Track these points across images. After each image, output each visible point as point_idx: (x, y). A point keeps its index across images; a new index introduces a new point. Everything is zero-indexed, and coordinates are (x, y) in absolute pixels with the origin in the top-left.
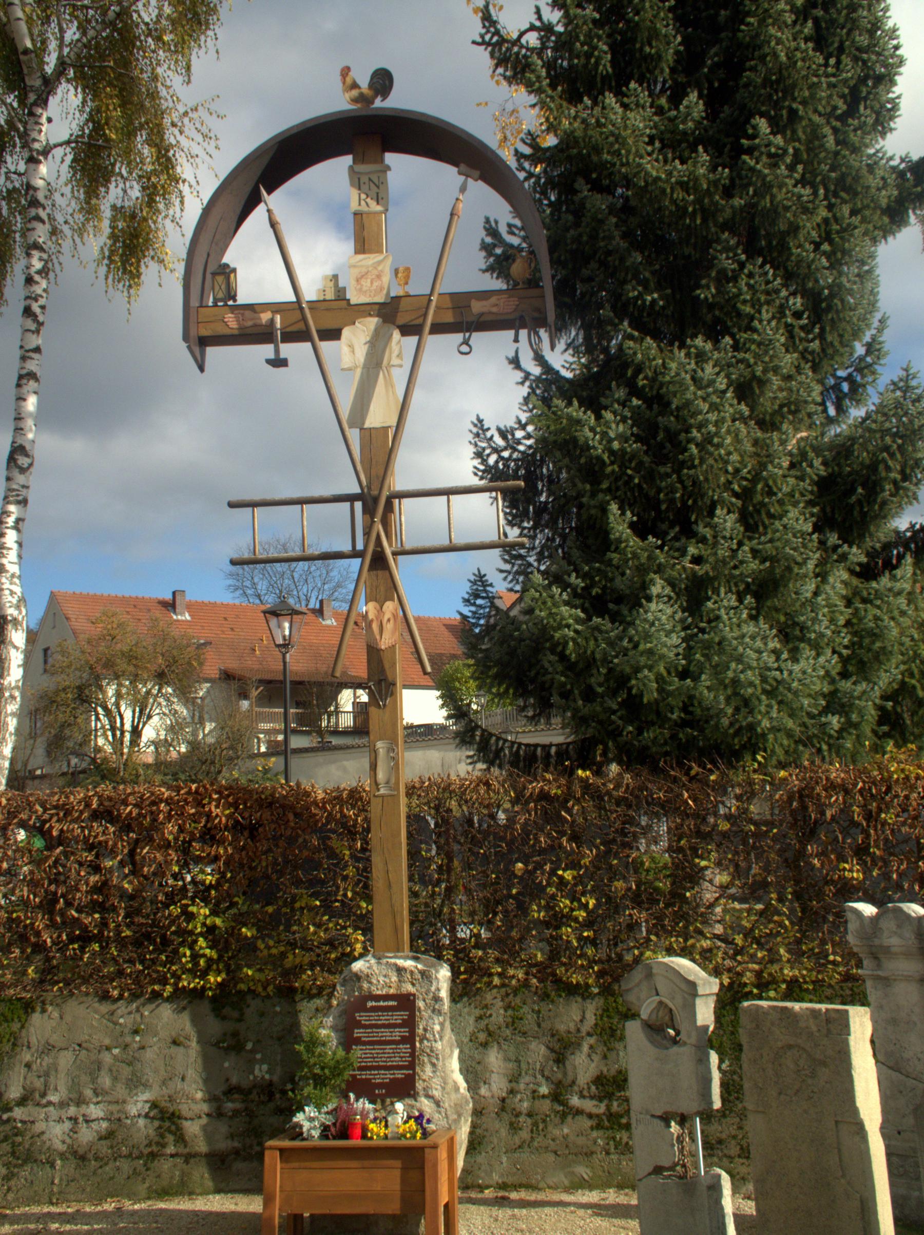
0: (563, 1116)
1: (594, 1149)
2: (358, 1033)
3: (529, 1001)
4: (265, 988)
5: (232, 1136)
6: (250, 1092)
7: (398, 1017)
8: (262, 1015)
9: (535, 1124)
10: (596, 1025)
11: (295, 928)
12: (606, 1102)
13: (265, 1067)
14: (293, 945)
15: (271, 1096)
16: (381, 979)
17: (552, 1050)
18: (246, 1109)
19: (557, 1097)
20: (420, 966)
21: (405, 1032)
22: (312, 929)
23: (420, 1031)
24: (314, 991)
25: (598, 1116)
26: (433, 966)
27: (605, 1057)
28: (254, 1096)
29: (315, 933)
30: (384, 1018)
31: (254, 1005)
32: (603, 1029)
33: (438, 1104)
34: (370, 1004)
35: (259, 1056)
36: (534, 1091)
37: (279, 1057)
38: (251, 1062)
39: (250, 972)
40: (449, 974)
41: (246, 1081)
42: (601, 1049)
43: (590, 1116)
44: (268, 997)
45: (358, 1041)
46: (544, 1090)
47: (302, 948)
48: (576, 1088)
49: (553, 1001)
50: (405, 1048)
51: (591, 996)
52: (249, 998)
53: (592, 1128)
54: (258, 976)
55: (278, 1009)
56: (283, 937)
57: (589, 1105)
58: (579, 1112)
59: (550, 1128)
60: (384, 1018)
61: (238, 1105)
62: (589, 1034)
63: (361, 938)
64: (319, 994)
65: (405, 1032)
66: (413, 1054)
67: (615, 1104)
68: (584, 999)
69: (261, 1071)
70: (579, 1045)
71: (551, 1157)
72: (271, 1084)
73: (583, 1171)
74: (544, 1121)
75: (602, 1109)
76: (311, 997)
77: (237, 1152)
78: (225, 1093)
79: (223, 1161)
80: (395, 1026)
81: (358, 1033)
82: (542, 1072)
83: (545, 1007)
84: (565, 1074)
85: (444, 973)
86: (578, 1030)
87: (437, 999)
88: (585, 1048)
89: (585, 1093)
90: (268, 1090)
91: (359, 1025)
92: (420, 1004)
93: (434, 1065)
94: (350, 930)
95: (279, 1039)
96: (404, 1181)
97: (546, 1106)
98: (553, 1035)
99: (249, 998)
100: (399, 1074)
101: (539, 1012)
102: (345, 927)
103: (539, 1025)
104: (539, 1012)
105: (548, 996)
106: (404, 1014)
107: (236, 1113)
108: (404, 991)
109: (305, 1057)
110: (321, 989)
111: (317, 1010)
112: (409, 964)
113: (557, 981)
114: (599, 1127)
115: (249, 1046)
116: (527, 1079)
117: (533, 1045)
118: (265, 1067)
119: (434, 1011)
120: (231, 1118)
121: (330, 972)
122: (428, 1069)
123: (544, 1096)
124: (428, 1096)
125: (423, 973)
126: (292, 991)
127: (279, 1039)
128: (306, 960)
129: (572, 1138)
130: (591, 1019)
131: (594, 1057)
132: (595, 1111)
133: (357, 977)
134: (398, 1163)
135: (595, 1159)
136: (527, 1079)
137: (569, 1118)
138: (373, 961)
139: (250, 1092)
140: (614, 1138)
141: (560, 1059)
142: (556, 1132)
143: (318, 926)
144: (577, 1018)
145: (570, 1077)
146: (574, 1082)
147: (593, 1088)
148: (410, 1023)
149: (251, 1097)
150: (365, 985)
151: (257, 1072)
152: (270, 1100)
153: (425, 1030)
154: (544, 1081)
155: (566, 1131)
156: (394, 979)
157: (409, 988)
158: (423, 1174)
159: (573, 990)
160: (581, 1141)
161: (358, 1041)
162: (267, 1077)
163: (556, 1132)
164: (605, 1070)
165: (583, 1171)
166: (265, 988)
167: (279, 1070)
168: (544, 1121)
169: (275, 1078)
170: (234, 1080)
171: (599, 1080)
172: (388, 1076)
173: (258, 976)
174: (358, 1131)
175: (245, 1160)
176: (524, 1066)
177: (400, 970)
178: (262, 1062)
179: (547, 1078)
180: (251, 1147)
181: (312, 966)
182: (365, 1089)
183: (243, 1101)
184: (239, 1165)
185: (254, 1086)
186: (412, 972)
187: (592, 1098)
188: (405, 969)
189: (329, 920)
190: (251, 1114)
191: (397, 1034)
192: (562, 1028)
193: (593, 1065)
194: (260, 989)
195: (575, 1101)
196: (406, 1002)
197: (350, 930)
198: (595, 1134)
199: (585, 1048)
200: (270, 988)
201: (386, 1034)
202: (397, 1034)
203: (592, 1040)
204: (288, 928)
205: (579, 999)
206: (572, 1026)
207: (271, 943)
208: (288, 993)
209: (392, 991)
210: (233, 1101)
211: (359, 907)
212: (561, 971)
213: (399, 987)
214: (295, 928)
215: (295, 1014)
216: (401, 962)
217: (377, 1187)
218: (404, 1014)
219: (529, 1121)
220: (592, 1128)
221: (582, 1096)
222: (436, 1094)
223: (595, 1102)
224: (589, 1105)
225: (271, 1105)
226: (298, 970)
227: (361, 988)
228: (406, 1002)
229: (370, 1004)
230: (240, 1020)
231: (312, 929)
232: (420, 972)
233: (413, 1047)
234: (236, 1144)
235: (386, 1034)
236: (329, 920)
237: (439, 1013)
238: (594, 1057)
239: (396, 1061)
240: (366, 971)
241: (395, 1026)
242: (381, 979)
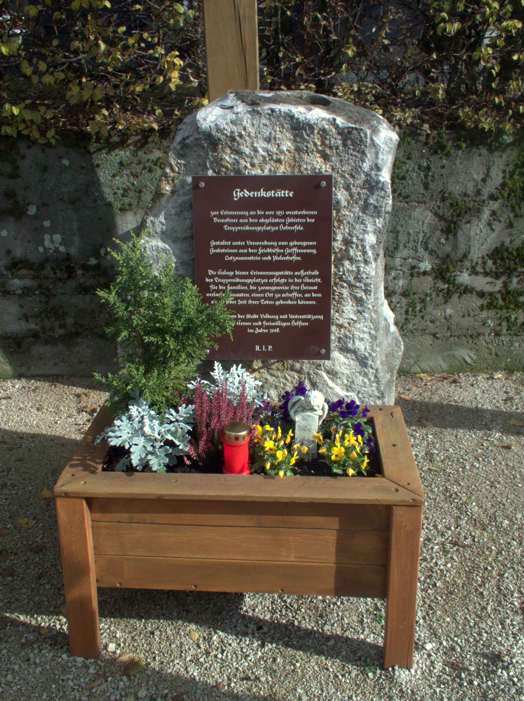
0: (447, 296)
1: (482, 330)
2: (216, 247)
3: (415, 154)
4: (43, 133)
5: (26, 318)
6: (42, 266)
7: (296, 220)
8: (45, 169)
9: (412, 305)
10: (503, 185)
11: (76, 44)
12: (503, 278)
13: (57, 237)
14: (79, 72)
15: (71, 273)
16: (260, 145)
17: (441, 218)
18: (40, 286)
19: (441, 273)
20: (339, 121)
21: (309, 247)
22: (103, 46)
23: (337, 245)
24: (116, 139)
25: (491, 294)
26: (362, 120)
27: (510, 225)
28: (48, 271)
29: (108, 53)
30: (268, 222)
31: (29, 159)
32: (512, 191)
33: (363, 361)
34: (239, 194)
35: (47, 224)
36: (413, 267)
37: (75, 226)
38: (38, 232)
39: (16, 111)
40: (395, 137)
41: (36, 254)
42: (506, 215)
43: (481, 294)
44: (49, 145)
45: (219, 262)
46: (426, 266)
47: (91, 76)
48: (467, 263)
49: (448, 155)
50: (310, 276)
51: (502, 148)
52: (22, 146)
53: (482, 308)
54: (28, 116)
55: (66, 162)
56: (60, 57)
57: (481, 283)
58: (467, 290)
59: (429, 309)
60: (268, 222)
61: (28, 283)
62: (492, 197)
63: (178, 62)
64: (122, 143)
65: (309, 247)
66: (325, 288)
67: (515, 280)
68: (491, 151)
69: (53, 242)
70: (479, 211)
71: (429, 340)
72: (68, 257)
73: (466, 354)
74: (423, 301)
75: (498, 285)
76: (111, 147)
77: (35, 336)
78: (8, 268)
79: (19, 345)
80: (289, 236)
81: (216, 247)
82: (425, 245)
83: (436, 163)
84: (455, 247)
85: (386, 136)
86: (478, 193)
87: (372, 185)
88: (486, 215)
89: (479, 269)
90: (66, 266)
91: (218, 232)
92: (341, 195)
93: (359, 301)
94: (161, 50)
95: (73, 202)
96: (342, 550)
97: (426, 284)
98: (443, 199)
99: (22, 146)
100: (298, 321)
101: (428, 168)
102: (151, 46)
103: (426, 187)
104: (428, 168)
105: (443, 148)
106: (309, 215)
107: (26, 292)
108: (306, 169)
109: (121, 311)
110: (124, 136)
111: (121, 164)
112: (317, 114)
113: (456, 126)
114: (490, 306)
115: (32, 210)
116: (405, 253)
117: (417, 213)
118: (57, 237)
119: (365, 208)
120: (20, 296)
121: (135, 112)
122: (349, 309)
123: (425, 273)
124: (344, 350)
125: (346, 134)
126: (83, 138)
127: (73, 202)
128: (99, 94)
129: (456, 319)
130: (497, 177)
131: (497, 226)
132: (488, 289)
133: (211, 141)
134: (334, 523)
135: (482, 342)
136: (405, 253)
137: (455, 297)
138: (241, 108)
139: (42, 266)
140: (508, 319)
141: (450, 228)
142: (438, 313)
143: (111, 43)
144: (478, 177)
145: (462, 248)
146: (465, 256)
147: (490, 262)
148: (321, 231)
149: (44, 273)
150: (228, 158)
151: (47, 243)
152: (70, 277)
153: (347, 242)
154: (426, 255)
155: (449, 311)
156: (287, 145)
157: (316, 163)
158: (387, 540)
159: (477, 138)
160: (467, 322)
161: (219, 262)
162: (62, 249)
163: (438, 313)
164: (507, 241)
165: (466, 354)
166: (43, 133)
167: (77, 242)
168: (423, 301)
169: (73, 251)
170: (18, 253)
171: (497, 254)
172: (279, 323)
173: (28, 116)
174: (242, 457)
175: (47, 343)
176: (403, 238)
177: (299, 128)
178: (52, 231)
179: (432, 252)
180: (52, 329)
181: (108, 102)
182: (238, 350)
183: (34, 278)
184: (39, 349)
185: (47, 260)
186: (324, 132)
187: (486, 274)
188: (309, 127)
189: (128, 33)
190: (47, 294)
191: (294, 251)
192: (456, 189)
193: (493, 235)
194: (36, 135)
195: (465, 278)
196: (313, 192)
197: (161, 50)
198: (484, 314)
199: (486, 215)
200: (51, 133)
201: (272, 251)
202: (294, 251)
203: (495, 205)
204: (65, 46)
205: (484, 151)
206: (470, 189)
207: (43, 66)
208: (78, 141)
209: (282, 170)
210: (20, 278)
211: (175, 14)
212: (464, 113)
213: (296, 163)
214: (76, 44)
215: (93, 168)
216: (300, 111)
217: (291, 558)
218: (309, 215)
219: (404, 301)
220: (482, 308)
221: (474, 272)
222: (360, 346)
223: (489, 279)
224: (481, 283)
225: (72, 283)
226: (87, 109)
227: (218, 162)
228: (313, 192)
229: (239, 194)
230: (14, 175)
231: (103, 46)
232: (341, 132)
233: (325, 275)
234: (32, 326)
235: (272, 251)
236: (128, 33)
237: (377, 211)
238: (497, 226)
239: (293, 298)
240: (229, 129)
241: (289, 236)
242: (260, 145)
